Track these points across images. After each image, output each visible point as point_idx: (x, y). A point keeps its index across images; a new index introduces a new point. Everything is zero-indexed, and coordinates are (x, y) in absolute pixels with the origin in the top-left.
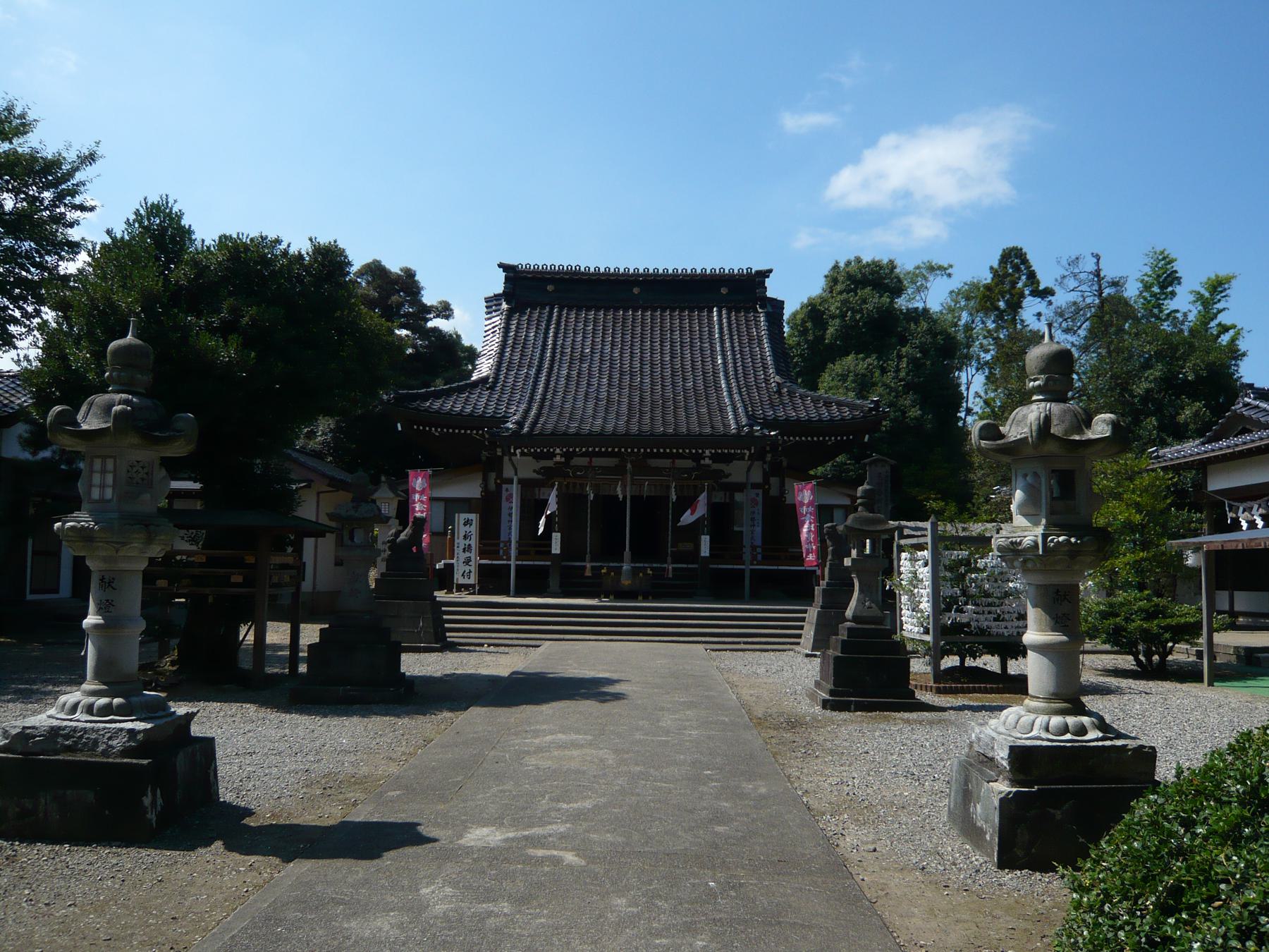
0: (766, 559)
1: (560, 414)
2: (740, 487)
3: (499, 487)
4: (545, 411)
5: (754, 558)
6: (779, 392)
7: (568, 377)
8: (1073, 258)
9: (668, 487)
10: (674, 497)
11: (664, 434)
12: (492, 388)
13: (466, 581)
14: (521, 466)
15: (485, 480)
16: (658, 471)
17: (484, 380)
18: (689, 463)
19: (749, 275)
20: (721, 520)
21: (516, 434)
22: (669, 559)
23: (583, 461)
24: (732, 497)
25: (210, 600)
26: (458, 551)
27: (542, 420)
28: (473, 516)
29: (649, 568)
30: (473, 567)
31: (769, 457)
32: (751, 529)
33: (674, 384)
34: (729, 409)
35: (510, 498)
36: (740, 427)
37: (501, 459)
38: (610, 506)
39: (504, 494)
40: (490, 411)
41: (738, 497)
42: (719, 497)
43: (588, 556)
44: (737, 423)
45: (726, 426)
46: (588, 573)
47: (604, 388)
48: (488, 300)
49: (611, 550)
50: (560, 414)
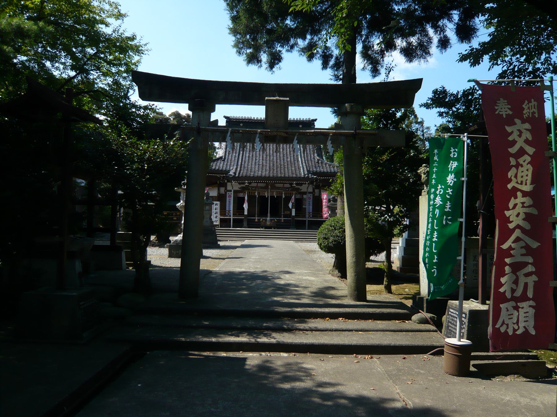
0: (313, 217)
1: (247, 170)
2: (305, 193)
3: (226, 193)
4: (242, 168)
5: (309, 216)
6: (318, 162)
7: (249, 156)
8: (467, 63)
9: (282, 193)
10: (284, 197)
11: (281, 177)
12: (224, 160)
14: (234, 186)
15: (219, 190)
16: (279, 188)
17: (221, 158)
18: (288, 186)
19: (309, 120)
20: (299, 204)
21: (234, 177)
23: (255, 185)
24: (302, 196)
27: (242, 172)
28: (218, 203)
30: (218, 219)
32: (309, 207)
33: (284, 159)
34: (302, 168)
35: (230, 196)
36: (305, 175)
37: (226, 183)
38: (263, 199)
39: (228, 195)
40: (224, 168)
41: (305, 196)
42: (298, 196)
44: (304, 173)
45: (300, 174)
46: (256, 221)
47: (261, 161)
49: (263, 213)
50: (247, 170)
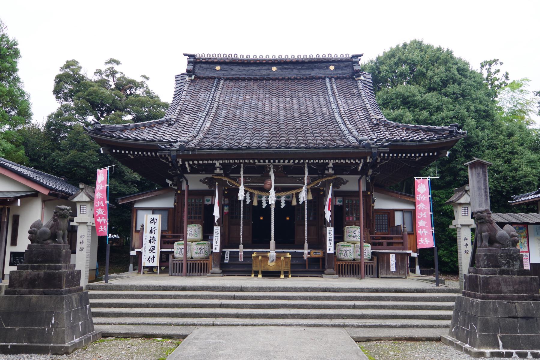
13: (151, 264)
22: (306, 245)
25: (9, 347)
26: (146, 242)
29: (288, 253)
30: (157, 254)
31: (370, 172)
43: (306, 245)
48: (194, 61)
